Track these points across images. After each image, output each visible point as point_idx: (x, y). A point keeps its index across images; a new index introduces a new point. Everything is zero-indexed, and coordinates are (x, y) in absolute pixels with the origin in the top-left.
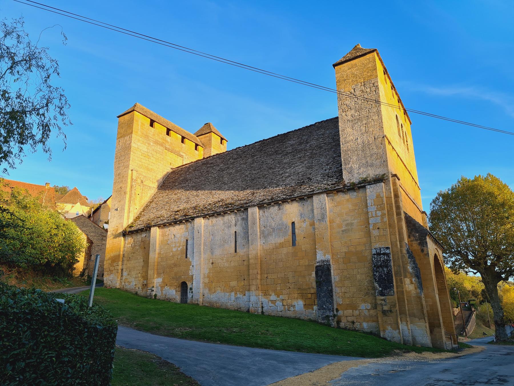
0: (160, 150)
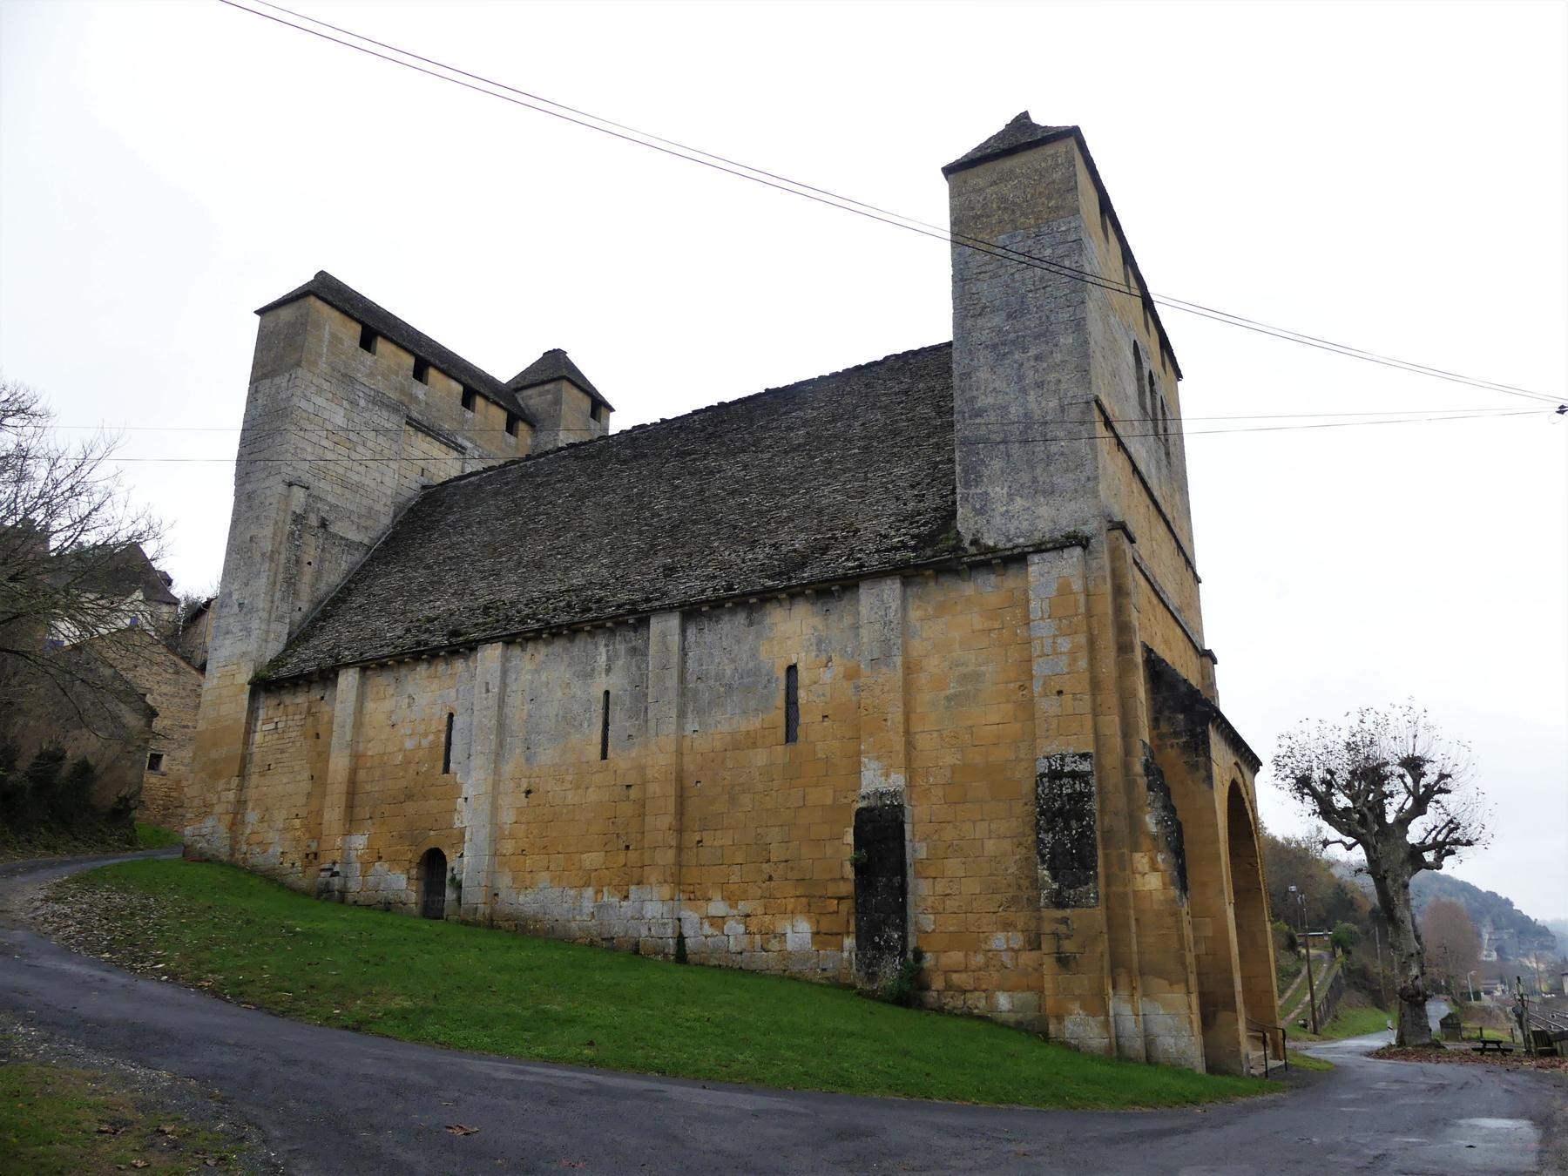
0: (388, 425)
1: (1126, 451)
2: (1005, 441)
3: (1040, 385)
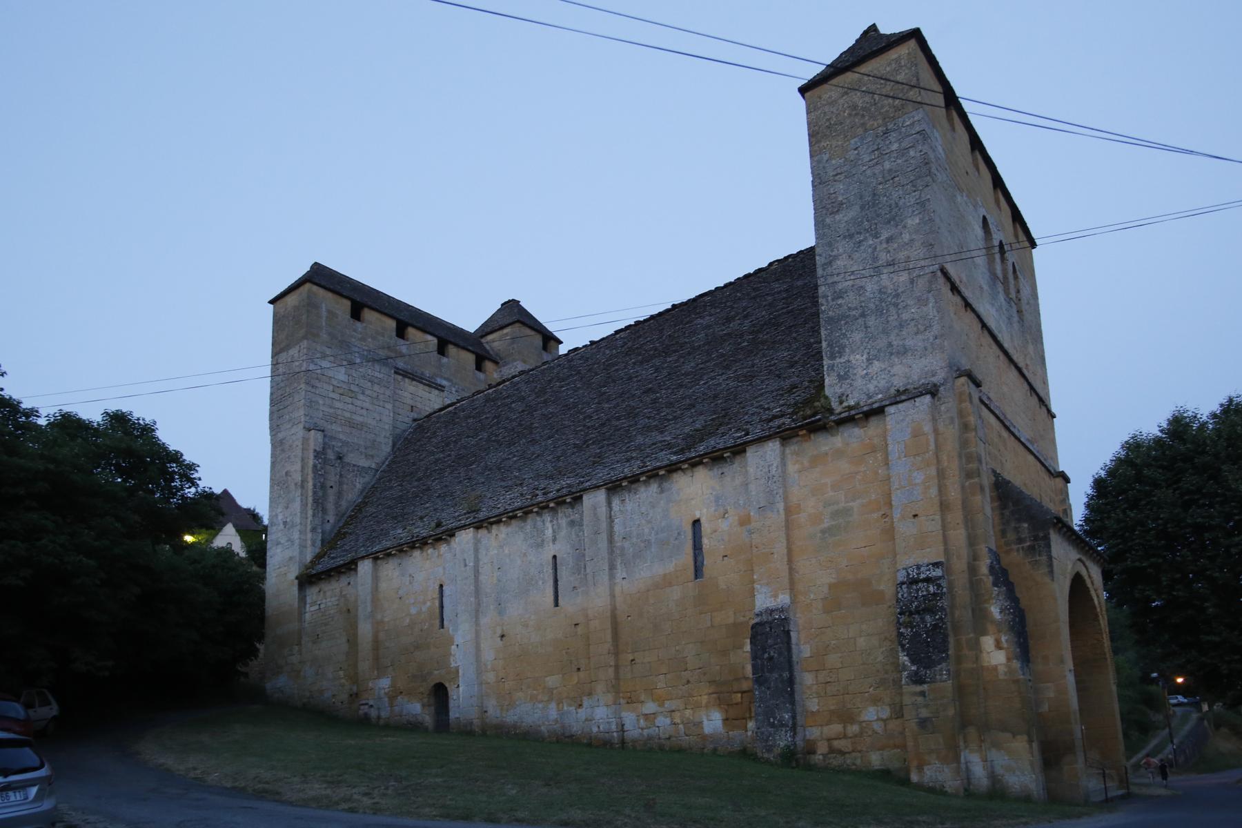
0: (381, 376)
1: (973, 310)
2: (863, 315)
3: (890, 264)
